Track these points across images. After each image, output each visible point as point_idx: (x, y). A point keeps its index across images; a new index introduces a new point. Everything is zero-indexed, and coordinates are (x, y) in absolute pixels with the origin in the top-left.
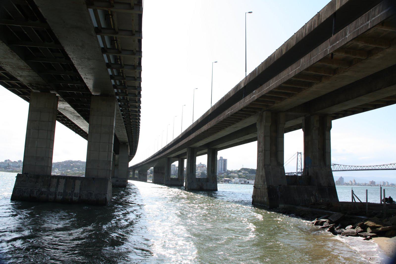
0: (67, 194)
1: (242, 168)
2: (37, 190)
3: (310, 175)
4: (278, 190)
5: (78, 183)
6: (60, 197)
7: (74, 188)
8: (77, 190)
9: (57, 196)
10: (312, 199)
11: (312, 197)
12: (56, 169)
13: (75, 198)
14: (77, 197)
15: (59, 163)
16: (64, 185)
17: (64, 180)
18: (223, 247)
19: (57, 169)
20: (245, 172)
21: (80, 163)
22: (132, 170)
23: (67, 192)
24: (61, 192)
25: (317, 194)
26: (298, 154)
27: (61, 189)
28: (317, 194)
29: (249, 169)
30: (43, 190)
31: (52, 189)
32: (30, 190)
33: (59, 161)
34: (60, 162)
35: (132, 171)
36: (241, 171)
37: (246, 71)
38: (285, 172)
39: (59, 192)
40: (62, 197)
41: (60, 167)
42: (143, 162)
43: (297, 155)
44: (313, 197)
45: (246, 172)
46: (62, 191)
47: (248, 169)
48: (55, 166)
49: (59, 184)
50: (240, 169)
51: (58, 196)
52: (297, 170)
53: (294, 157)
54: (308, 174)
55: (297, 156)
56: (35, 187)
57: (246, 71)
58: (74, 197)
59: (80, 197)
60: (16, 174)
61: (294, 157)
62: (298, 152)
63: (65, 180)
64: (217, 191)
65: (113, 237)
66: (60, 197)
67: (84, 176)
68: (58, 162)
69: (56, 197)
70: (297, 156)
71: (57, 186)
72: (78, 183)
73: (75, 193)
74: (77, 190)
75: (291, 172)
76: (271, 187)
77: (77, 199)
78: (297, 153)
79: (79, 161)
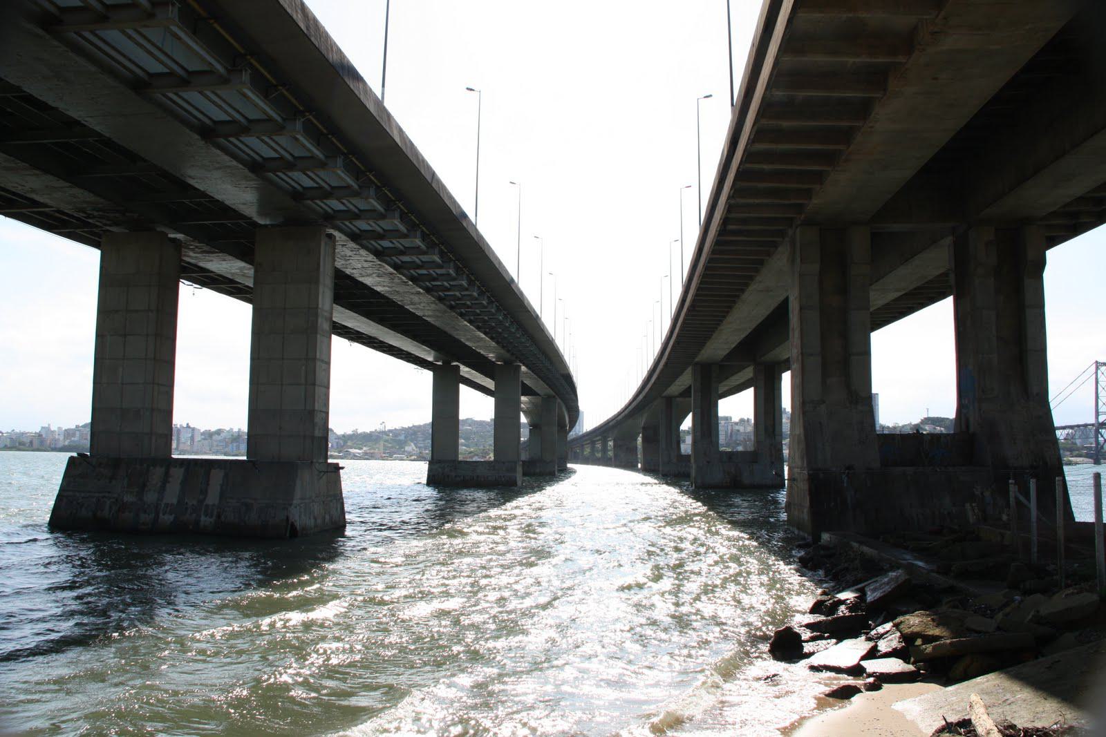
0: (186, 509)
1: (926, 416)
2: (111, 500)
3: (972, 430)
4: (845, 485)
5: (217, 477)
6: (167, 519)
7: (204, 492)
8: (212, 498)
9: (161, 515)
10: (970, 513)
11: (971, 505)
12: (410, 445)
13: (205, 520)
14: (211, 517)
15: (415, 429)
16: (181, 484)
17: (182, 470)
18: (574, 705)
19: (412, 444)
20: (935, 428)
21: (470, 426)
22: (600, 437)
23: (187, 503)
24: (172, 505)
25: (987, 494)
26: (1097, 368)
27: (172, 495)
28: (987, 494)
29: (948, 419)
30: (129, 498)
31: (150, 497)
32: (94, 500)
33: (416, 424)
34: (419, 427)
35: (599, 440)
36: (922, 426)
37: (476, 216)
38: (1055, 425)
39: (167, 505)
40: (172, 518)
41: (421, 439)
42: (619, 414)
43: (1094, 371)
44: (974, 505)
45: (939, 428)
46: (175, 501)
47: (944, 419)
48: (405, 437)
49: (169, 482)
50: (920, 420)
51: (164, 515)
52: (1097, 417)
53: (1083, 378)
54: (967, 427)
55: (1096, 373)
56: (109, 492)
57: (476, 216)
58: (203, 518)
59: (219, 516)
60: (65, 457)
61: (1083, 378)
62: (1097, 362)
63: (182, 470)
64: (517, 485)
65: (624, 675)
66: (166, 517)
67: (491, 457)
68: (414, 426)
69: (158, 517)
70: (1096, 373)
71: (163, 488)
72: (217, 477)
73: (207, 506)
74: (212, 498)
75: (1076, 424)
76: (821, 475)
77: (211, 522)
78: (1094, 365)
79: (467, 419)
